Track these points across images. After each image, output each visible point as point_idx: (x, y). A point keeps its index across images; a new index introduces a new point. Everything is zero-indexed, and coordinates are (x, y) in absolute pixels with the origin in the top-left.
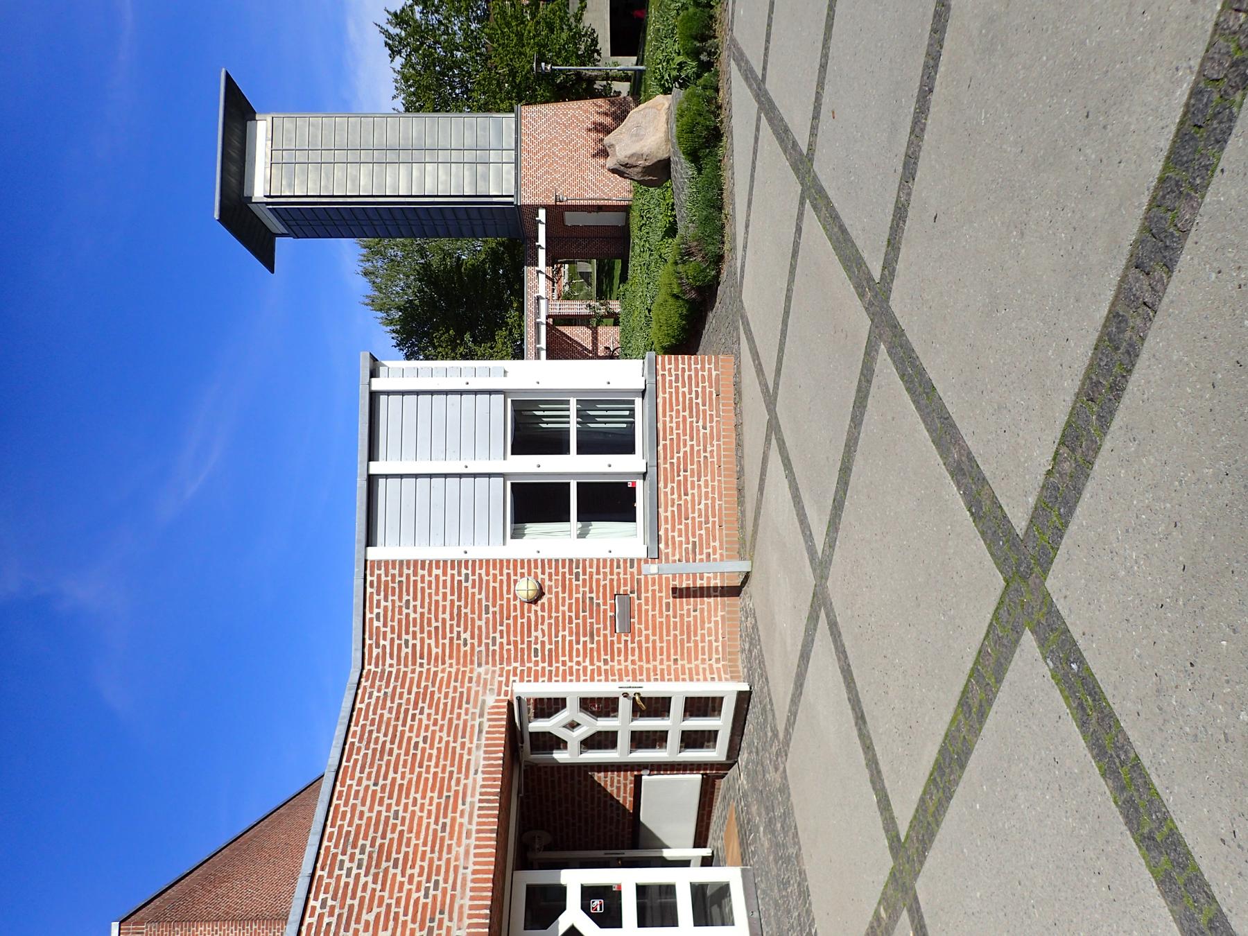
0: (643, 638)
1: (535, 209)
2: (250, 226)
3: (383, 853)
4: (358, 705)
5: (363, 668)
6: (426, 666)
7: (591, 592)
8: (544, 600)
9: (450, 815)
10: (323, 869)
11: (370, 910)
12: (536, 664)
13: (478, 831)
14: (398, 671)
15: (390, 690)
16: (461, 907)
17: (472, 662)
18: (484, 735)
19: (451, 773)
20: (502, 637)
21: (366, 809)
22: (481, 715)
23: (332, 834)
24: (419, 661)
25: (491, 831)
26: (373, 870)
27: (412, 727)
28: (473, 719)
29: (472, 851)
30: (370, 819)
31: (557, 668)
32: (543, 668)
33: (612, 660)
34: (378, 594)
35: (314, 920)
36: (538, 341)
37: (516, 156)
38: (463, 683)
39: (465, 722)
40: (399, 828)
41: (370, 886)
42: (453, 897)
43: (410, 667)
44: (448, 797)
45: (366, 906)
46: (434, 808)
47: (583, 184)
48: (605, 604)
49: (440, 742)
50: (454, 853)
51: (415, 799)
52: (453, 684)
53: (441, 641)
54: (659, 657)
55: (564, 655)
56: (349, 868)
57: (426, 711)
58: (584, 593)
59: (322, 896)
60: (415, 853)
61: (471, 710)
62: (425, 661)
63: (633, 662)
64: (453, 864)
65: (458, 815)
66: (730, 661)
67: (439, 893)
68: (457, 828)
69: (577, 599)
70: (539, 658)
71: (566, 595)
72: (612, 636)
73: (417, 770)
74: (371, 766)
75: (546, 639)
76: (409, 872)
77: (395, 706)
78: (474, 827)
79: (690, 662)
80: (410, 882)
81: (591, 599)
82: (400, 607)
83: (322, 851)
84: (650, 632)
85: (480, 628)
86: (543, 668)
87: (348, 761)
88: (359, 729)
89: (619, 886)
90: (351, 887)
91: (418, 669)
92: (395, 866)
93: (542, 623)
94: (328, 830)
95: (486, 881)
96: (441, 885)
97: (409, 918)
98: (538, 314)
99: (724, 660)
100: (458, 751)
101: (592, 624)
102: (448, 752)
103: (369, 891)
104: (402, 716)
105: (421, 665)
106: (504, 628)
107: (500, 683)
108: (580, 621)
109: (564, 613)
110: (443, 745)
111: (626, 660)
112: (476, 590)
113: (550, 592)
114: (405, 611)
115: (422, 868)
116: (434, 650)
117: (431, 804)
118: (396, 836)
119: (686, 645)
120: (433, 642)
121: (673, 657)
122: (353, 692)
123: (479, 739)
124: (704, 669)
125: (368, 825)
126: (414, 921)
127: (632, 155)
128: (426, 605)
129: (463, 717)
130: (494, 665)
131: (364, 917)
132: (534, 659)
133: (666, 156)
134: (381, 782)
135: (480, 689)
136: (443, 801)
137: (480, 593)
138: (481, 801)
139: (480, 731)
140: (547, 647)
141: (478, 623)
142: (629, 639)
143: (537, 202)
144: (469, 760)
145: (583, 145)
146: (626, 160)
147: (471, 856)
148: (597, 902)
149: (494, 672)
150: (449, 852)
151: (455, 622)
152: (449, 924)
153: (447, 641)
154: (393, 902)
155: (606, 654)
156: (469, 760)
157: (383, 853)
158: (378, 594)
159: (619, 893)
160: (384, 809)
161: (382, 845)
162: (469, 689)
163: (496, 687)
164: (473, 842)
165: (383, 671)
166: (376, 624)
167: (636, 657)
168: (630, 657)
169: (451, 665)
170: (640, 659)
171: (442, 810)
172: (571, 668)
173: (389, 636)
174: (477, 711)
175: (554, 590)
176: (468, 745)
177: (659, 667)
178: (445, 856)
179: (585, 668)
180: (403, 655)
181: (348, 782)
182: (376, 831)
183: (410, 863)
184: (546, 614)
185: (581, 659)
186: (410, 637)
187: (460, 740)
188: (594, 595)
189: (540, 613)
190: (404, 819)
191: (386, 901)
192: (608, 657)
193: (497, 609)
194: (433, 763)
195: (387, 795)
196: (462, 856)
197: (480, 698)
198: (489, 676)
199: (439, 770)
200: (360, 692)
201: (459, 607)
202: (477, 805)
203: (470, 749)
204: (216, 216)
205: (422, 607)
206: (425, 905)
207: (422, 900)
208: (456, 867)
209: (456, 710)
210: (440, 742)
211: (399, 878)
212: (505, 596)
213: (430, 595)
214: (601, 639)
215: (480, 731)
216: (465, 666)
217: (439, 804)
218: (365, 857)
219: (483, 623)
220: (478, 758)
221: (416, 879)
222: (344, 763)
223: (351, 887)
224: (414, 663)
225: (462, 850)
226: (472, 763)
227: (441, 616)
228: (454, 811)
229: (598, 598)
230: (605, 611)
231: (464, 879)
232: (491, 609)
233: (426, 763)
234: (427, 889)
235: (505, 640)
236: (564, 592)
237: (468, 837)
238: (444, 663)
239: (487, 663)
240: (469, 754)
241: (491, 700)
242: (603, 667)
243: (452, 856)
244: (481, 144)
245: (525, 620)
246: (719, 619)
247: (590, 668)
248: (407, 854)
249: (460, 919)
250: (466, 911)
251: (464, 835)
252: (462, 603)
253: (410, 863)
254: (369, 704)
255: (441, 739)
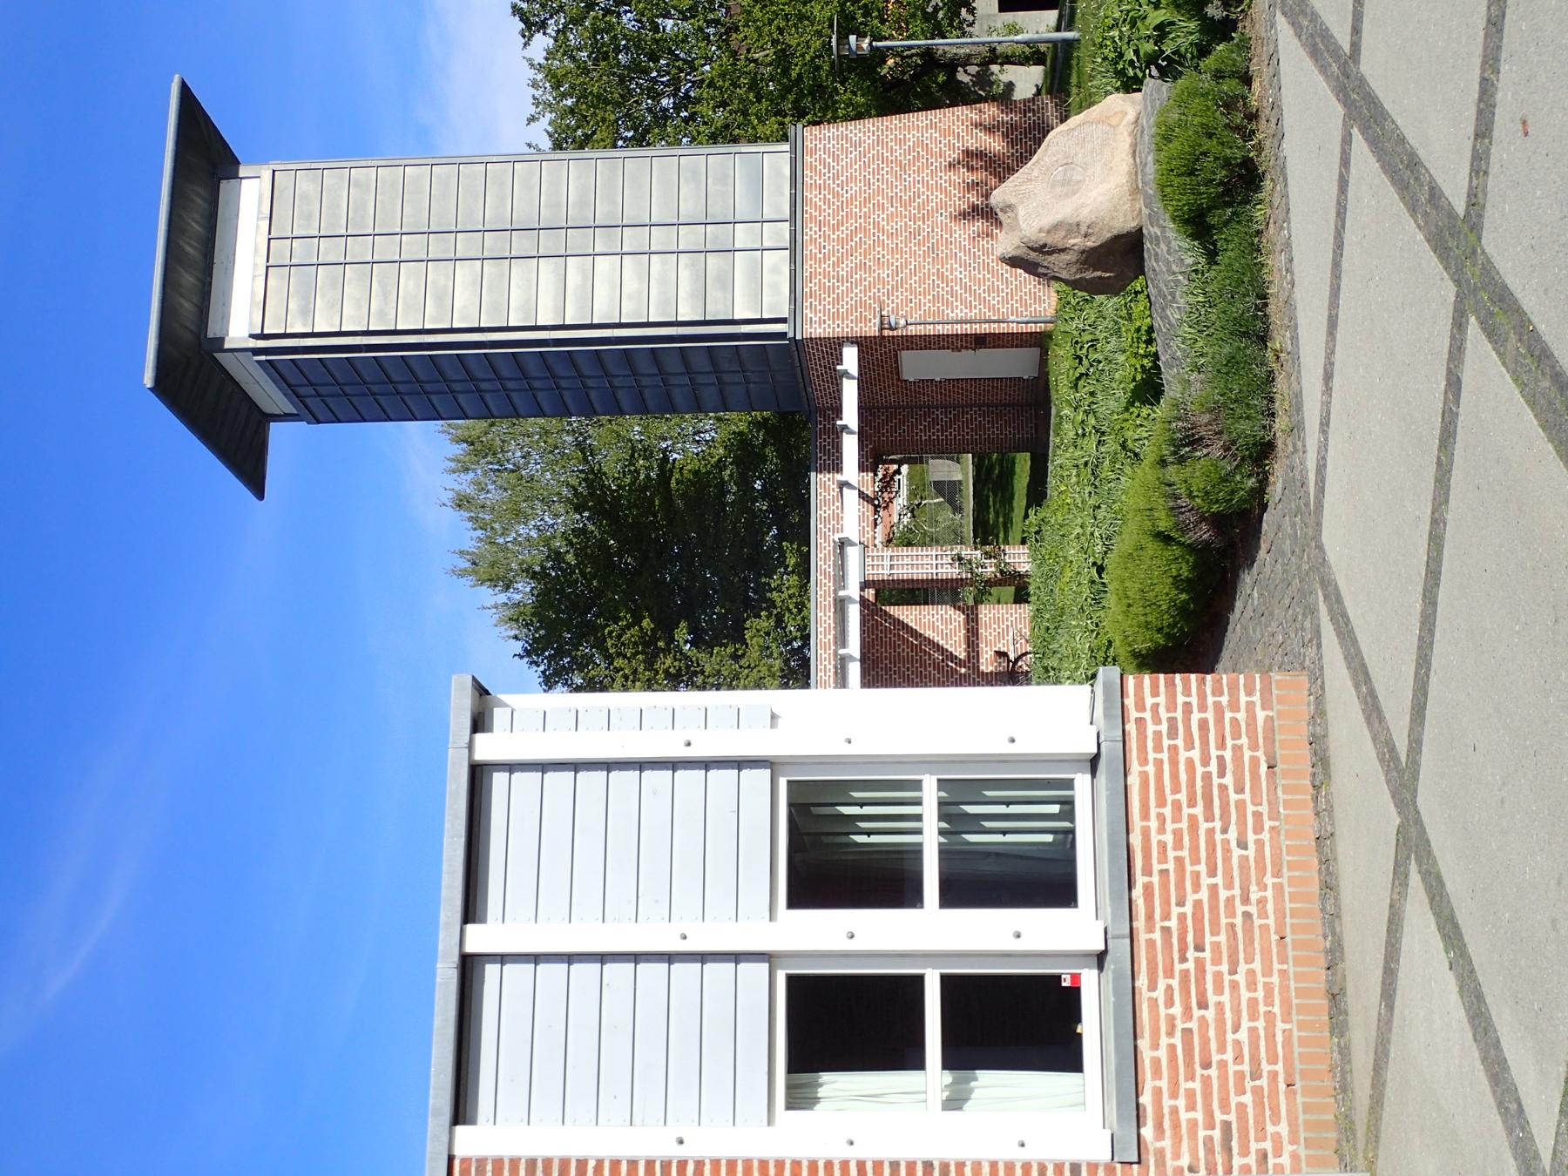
1: (833, 347)
2: (218, 403)
36: (841, 639)
37: (793, 234)
47: (943, 289)
98: (841, 579)
127: (1056, 227)
133: (1131, 225)
143: (839, 332)
145: (940, 205)
146: (1043, 238)
204: (148, 379)
244: (716, 212)
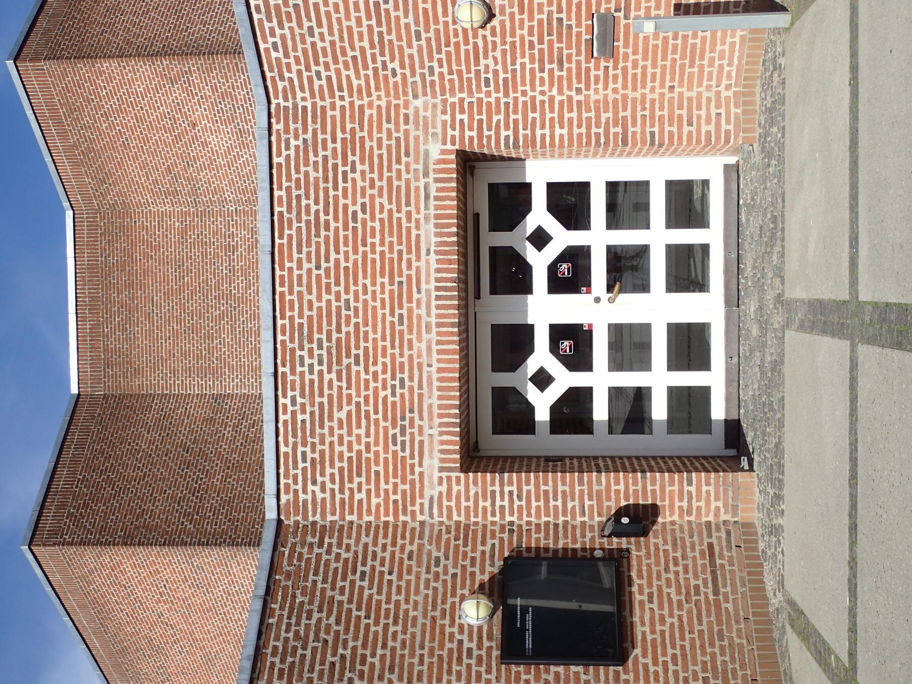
0: (629, 65)
3: (341, 350)
4: (276, 160)
5: (269, 102)
6: (347, 99)
7: (560, 11)
8: (495, 22)
9: (405, 305)
10: (284, 365)
11: (340, 408)
12: (488, 94)
13: (439, 325)
14: (314, 105)
15: (309, 136)
16: (430, 406)
17: (405, 94)
18: (432, 203)
19: (400, 252)
20: (441, 66)
21: (313, 297)
22: (426, 175)
23: (284, 326)
24: (337, 94)
25: (452, 325)
26: (335, 368)
27: (345, 190)
28: (417, 179)
29: (435, 348)
30: (320, 309)
31: (516, 99)
32: (498, 100)
33: (588, 88)
34: (270, 20)
35: (288, 417)
38: (397, 124)
39: (408, 182)
40: (353, 321)
41: (336, 383)
42: (421, 396)
43: (328, 100)
44: (401, 283)
45: (335, 404)
46: (386, 296)
48: (579, 25)
49: (381, 212)
50: (415, 348)
51: (365, 285)
52: (385, 126)
53: (362, 72)
54: (649, 85)
55: (523, 84)
56: (310, 364)
57: (359, 167)
58: (550, 14)
59: (290, 394)
60: (375, 348)
61: (413, 166)
62: (346, 94)
63: (615, 91)
64: (416, 361)
65: (414, 305)
66: (745, 86)
67: (406, 391)
68: (415, 321)
69: (540, 22)
70: (492, 88)
71: (525, 16)
72: (588, 62)
73: (361, 249)
74: (309, 244)
75: (499, 67)
76: (372, 369)
77: (320, 159)
78: (433, 320)
79: (690, 89)
80: (375, 379)
81: (560, 20)
82: (302, 36)
83: (279, 346)
84: (639, 57)
85: (411, 57)
86: (498, 100)
87: (281, 237)
88: (283, 193)
89: (590, 325)
90: (316, 384)
91: (339, 103)
92: (357, 363)
93: (494, 50)
94: (279, 322)
95: (452, 380)
96: (407, 383)
97: (380, 416)
99: (736, 86)
100: (404, 224)
101: (560, 49)
102: (391, 225)
103: (335, 389)
104: (331, 175)
105: (342, 98)
106: (443, 56)
107: (444, 123)
108: (545, 46)
109: (522, 38)
110: (385, 215)
111: (605, 88)
112: (401, 13)
113: (502, 12)
114: (309, 40)
115: (384, 364)
116: (355, 83)
117: (383, 292)
118: (351, 329)
119: (687, 70)
120: (352, 73)
121: (668, 84)
122: (266, 142)
123: (427, 207)
124: (709, 99)
125: (320, 317)
126: (385, 419)
128: (336, 32)
129: (404, 176)
130: (434, 96)
131: (336, 415)
132: (484, 89)
134: (324, 265)
135: (420, 133)
136: (395, 287)
137: (406, 16)
138: (437, 289)
139: (427, 197)
140: (502, 76)
141: (407, 51)
142: (611, 65)
144: (418, 236)
147: (434, 353)
148: (566, 343)
149: (435, 106)
150: (410, 348)
151: (377, 51)
152: (421, 423)
153: (370, 72)
154: (362, 400)
155: (579, 82)
156: (418, 236)
157: (341, 350)
158: (270, 20)
159: (590, 332)
160: (332, 297)
161: (339, 340)
162: (407, 132)
163: (439, 130)
164: (434, 337)
165: (295, 106)
166: (274, 55)
167: (619, 85)
168: (611, 86)
169: (379, 98)
170: (625, 87)
171: (396, 300)
172: (533, 98)
173: (294, 68)
174: (420, 167)
175: (508, 11)
176: (414, 216)
177: (649, 97)
178: (407, 353)
179: (552, 99)
180: (316, 88)
181: (287, 265)
182: (329, 323)
183: (371, 360)
184: (498, 40)
185: (546, 88)
186: (321, 68)
187: (404, 209)
188: (563, 15)
189: (490, 39)
190: (356, 309)
191: (355, 399)
192: (582, 86)
193: (432, 34)
194: (377, 240)
195: (351, 635)
196: (424, 353)
197: (422, 148)
198: (429, 114)
199: (386, 249)
200: (273, 138)
201: (380, 34)
202: (434, 294)
203: (417, 221)
205: (331, 33)
206: (394, 404)
207: (390, 399)
208: (420, 365)
209: (395, 166)
210: (381, 212)
211: (363, 376)
212: (441, 19)
213: (339, 20)
214: (574, 66)
215: (427, 197)
216: (397, 97)
217: (392, 292)
218: (324, 352)
219: (414, 51)
220: (428, 234)
221: (381, 377)
222: (277, 241)
223: (316, 384)
224: (332, 95)
225: (423, 346)
226: (423, 239)
227: (357, 44)
228: (410, 300)
229: (569, 19)
230: (579, 34)
231: (430, 377)
232: (424, 35)
233: (369, 240)
234: (393, 387)
235: (445, 70)
236: (521, 12)
237: (428, 331)
238: (369, 95)
239: (425, 94)
240: (418, 227)
241: (435, 150)
242: (576, 98)
243: (414, 352)
245: (470, 47)
246: (737, 40)
247: (558, 98)
248: (366, 349)
249: (431, 419)
250: (436, 411)
251: (424, 329)
252: (384, 29)
253: (371, 360)
254: (288, 156)
255: (382, 206)
